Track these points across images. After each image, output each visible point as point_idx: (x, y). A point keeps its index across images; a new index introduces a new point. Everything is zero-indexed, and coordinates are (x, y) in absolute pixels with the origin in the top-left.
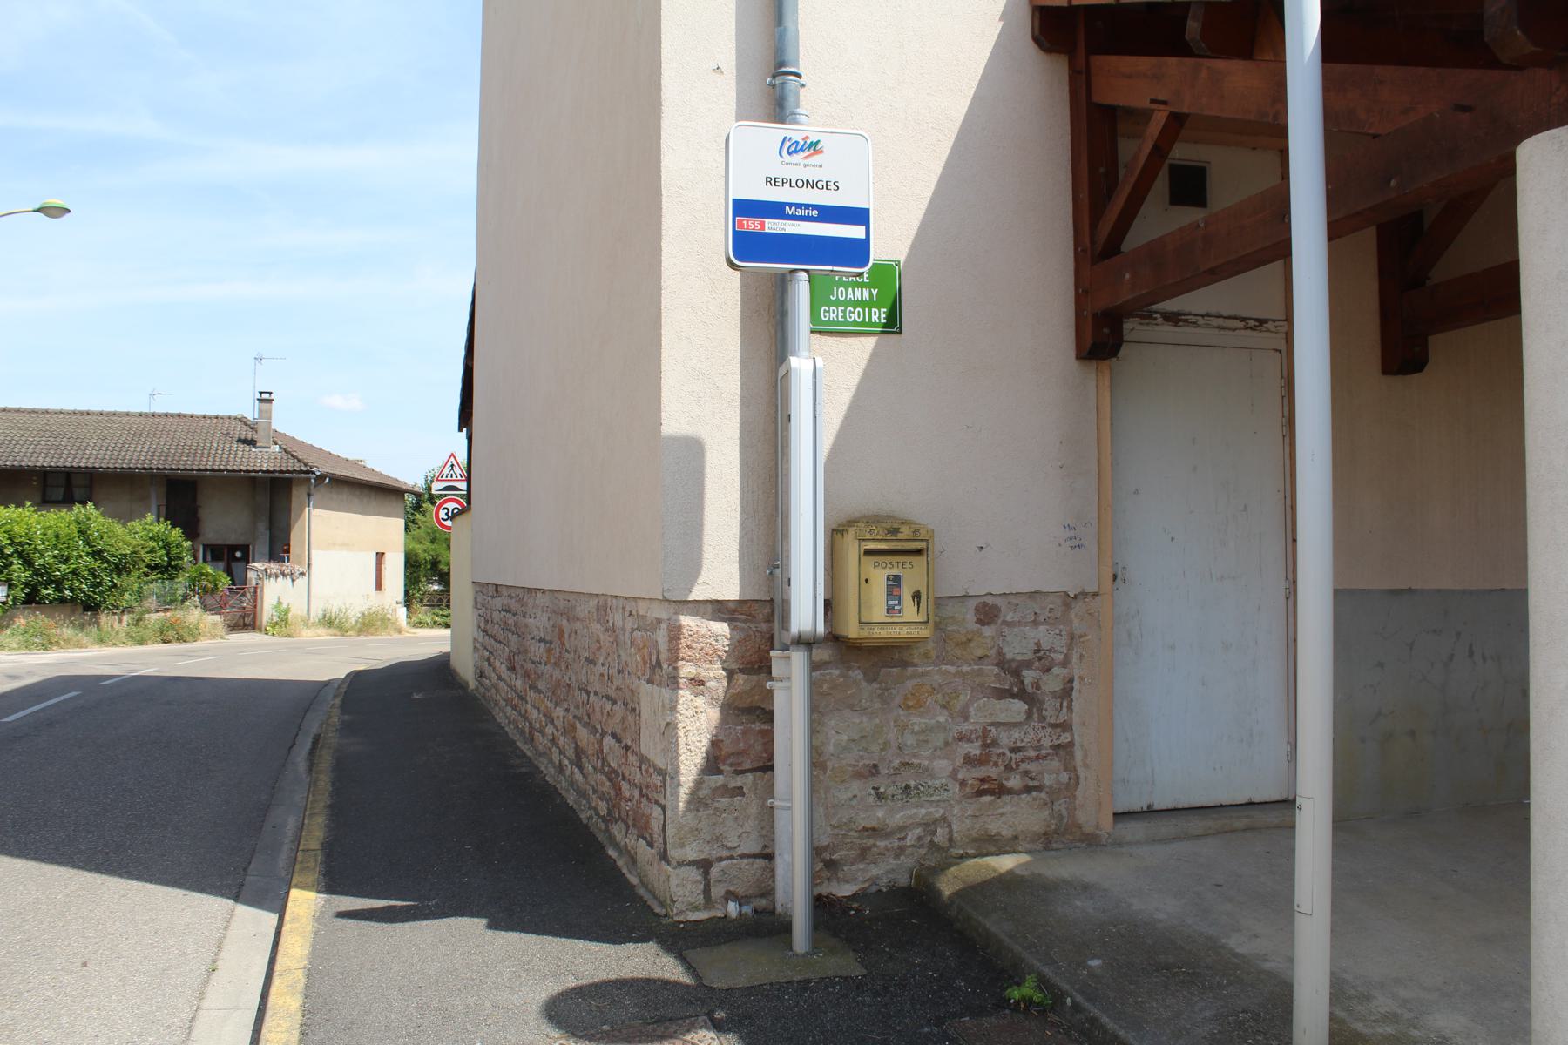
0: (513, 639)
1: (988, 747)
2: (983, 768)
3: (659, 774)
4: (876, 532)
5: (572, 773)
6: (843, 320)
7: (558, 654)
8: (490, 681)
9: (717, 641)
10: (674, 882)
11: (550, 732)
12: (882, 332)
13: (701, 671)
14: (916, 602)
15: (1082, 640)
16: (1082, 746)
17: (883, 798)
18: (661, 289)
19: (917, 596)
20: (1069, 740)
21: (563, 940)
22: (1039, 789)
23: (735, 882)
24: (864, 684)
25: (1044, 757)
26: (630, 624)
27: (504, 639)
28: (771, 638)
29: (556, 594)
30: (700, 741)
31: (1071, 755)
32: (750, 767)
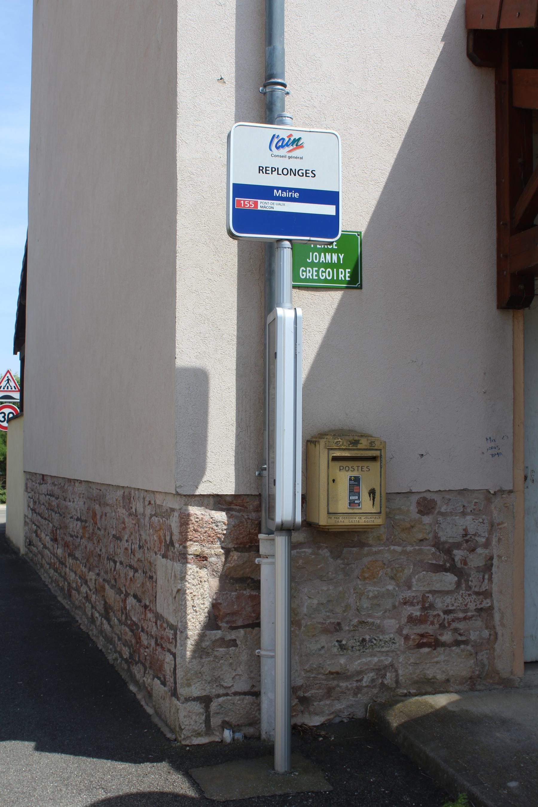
0: (56, 517)
1: (427, 610)
2: (423, 626)
3: (171, 629)
4: (341, 443)
5: (102, 623)
6: (317, 278)
7: (91, 531)
8: (37, 548)
9: (217, 526)
10: (182, 714)
11: (84, 591)
12: (347, 288)
13: (205, 549)
14: (372, 498)
15: (500, 527)
16: (500, 609)
17: (345, 649)
18: (176, 253)
19: (372, 492)
20: (489, 605)
21: (95, 760)
22: (466, 642)
23: (229, 714)
24: (331, 560)
25: (470, 618)
26: (149, 511)
27: (49, 516)
28: (259, 524)
29: (90, 485)
30: (203, 604)
31: (491, 616)
32: (242, 624)
